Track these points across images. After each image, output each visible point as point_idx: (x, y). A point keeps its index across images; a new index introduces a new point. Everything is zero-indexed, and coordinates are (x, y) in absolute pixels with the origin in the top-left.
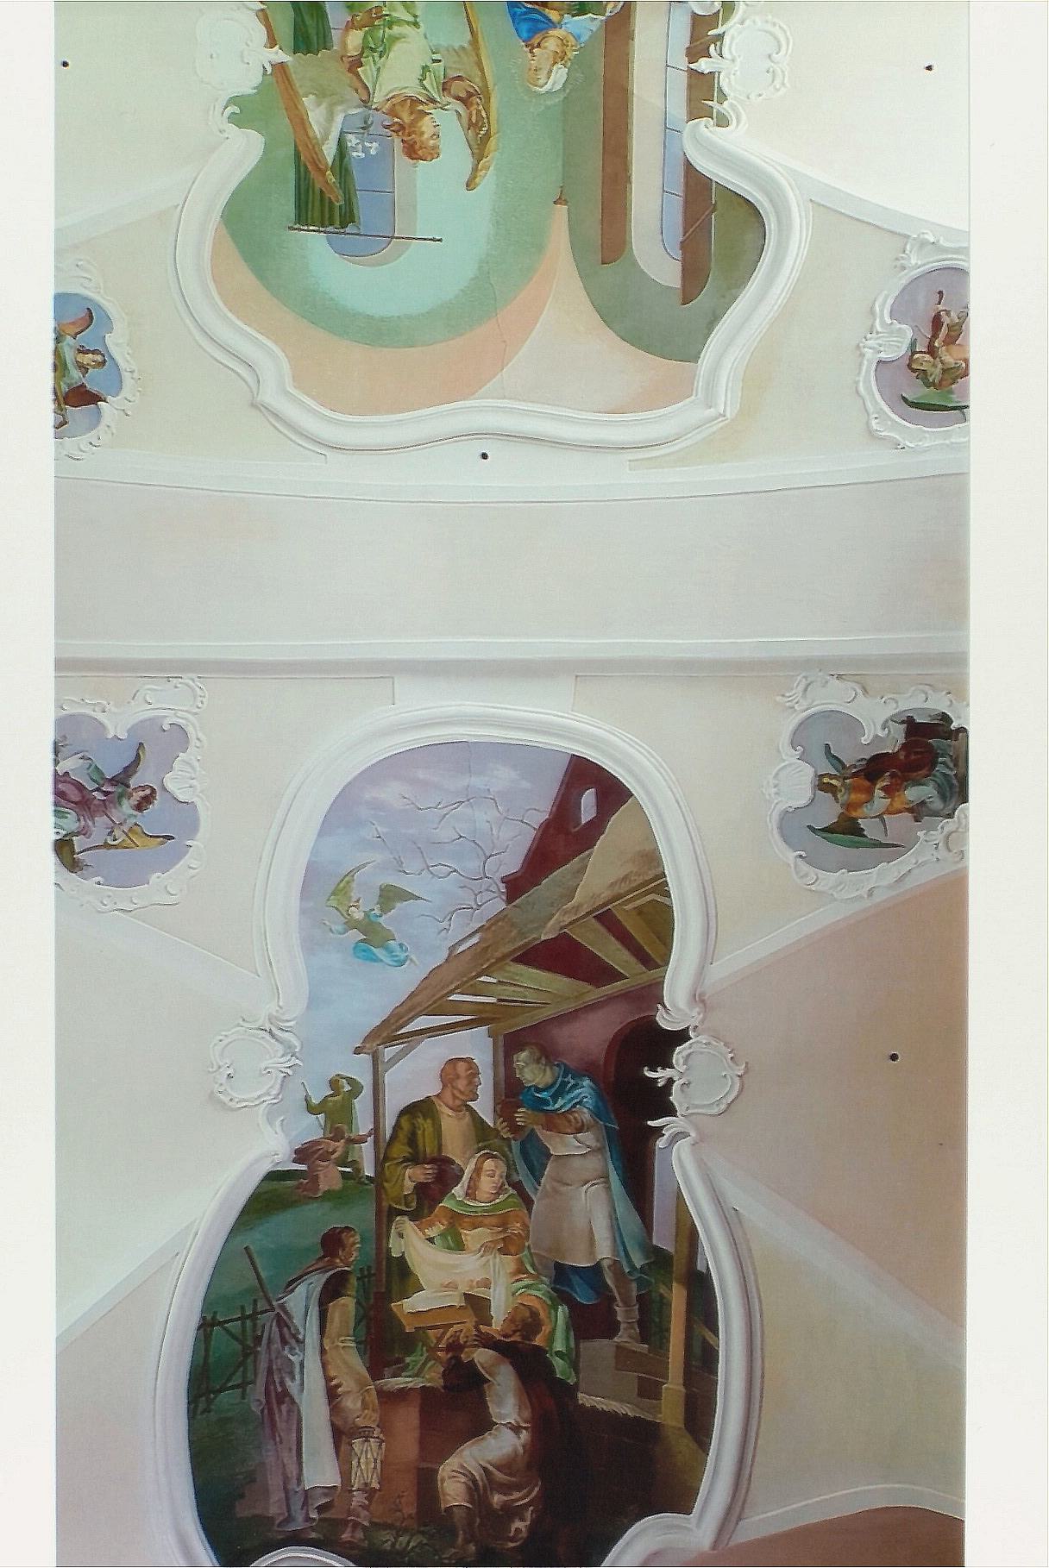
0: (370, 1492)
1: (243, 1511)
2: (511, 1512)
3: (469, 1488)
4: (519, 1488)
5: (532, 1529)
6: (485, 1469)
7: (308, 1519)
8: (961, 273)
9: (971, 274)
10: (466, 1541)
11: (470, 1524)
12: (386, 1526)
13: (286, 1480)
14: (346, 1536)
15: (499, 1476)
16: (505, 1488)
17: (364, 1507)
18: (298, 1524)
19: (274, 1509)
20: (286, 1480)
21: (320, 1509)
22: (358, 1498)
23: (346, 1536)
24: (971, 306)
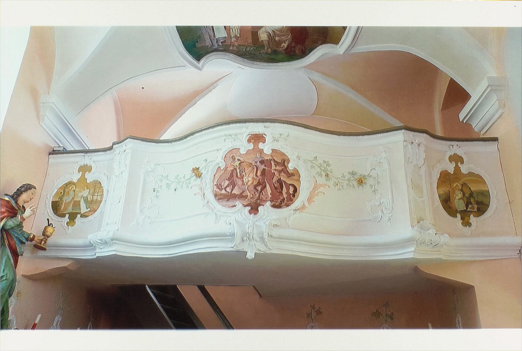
0: (236, 37)
1: (198, 45)
2: (280, 42)
3: (268, 36)
4: (284, 36)
5: (288, 46)
6: (273, 31)
7: (218, 45)
8: (470, 322)
9: (361, 25)
10: (268, 48)
11: (269, 44)
12: (243, 45)
13: (210, 37)
14: (231, 48)
15: (278, 33)
16: (279, 36)
17: (235, 41)
18: (216, 46)
19: (208, 43)
20: (210, 37)
21: (222, 43)
22: (233, 40)
23: (231, 48)
24: (166, 25)
